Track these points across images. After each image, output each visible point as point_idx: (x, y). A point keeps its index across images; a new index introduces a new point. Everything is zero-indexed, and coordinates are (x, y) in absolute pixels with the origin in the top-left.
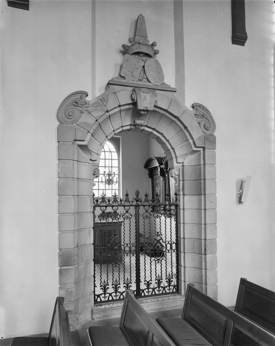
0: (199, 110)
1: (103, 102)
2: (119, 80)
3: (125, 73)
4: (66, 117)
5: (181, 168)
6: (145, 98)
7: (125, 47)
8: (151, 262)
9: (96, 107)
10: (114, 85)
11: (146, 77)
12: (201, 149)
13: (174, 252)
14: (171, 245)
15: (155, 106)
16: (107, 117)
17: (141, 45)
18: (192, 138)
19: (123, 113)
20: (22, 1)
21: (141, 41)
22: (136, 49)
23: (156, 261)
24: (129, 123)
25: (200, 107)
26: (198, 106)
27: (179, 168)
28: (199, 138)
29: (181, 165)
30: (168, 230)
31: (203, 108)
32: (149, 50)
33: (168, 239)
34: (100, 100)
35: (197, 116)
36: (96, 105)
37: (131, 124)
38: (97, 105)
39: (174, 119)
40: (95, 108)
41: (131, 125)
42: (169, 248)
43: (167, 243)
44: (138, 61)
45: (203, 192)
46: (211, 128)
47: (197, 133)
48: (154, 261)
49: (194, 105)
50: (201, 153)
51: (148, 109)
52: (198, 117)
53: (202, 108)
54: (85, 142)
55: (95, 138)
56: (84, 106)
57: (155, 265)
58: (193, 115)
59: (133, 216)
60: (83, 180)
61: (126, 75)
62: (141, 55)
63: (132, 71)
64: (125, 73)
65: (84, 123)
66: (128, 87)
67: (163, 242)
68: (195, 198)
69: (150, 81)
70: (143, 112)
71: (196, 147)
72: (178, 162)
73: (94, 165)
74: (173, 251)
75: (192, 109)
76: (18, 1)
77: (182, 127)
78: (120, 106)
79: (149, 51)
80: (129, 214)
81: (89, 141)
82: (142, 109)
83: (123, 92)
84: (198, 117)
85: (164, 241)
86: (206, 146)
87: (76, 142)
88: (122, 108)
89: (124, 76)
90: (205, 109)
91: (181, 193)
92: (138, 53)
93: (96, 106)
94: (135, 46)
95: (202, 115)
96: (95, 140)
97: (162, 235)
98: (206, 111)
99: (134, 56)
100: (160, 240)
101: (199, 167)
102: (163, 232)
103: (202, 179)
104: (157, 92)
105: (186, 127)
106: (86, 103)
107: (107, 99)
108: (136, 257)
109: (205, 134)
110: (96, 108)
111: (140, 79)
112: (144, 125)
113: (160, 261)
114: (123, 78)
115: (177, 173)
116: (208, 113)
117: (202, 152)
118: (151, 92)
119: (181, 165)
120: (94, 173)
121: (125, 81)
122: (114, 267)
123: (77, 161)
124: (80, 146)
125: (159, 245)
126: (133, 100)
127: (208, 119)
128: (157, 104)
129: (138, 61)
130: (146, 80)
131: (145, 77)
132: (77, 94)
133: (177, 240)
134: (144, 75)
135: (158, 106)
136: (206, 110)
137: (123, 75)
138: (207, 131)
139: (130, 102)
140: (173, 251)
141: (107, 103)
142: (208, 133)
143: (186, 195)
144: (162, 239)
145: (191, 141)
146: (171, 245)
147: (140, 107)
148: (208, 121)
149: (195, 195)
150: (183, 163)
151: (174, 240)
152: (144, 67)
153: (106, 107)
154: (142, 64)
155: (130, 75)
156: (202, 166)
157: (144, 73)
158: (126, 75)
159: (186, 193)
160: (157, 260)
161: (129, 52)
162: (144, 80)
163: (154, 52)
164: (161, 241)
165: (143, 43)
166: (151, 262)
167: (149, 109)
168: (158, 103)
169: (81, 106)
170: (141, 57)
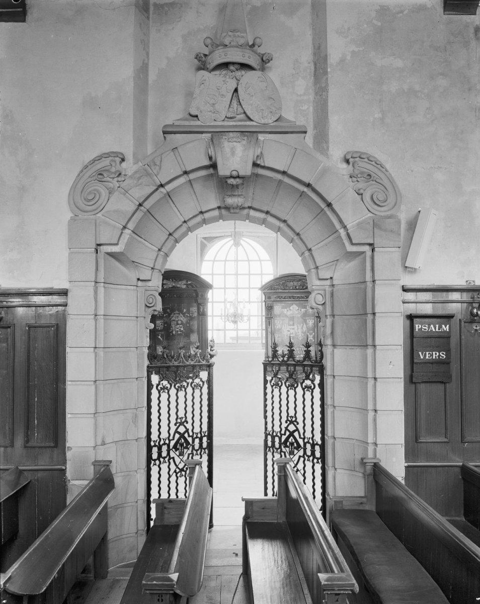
0: (361, 164)
1: (152, 168)
2: (187, 123)
3: (198, 108)
4: (91, 205)
5: (328, 289)
6: (233, 153)
7: (199, 58)
8: (170, 476)
9: (139, 178)
10: (175, 133)
11: (242, 111)
12: (367, 249)
13: (205, 452)
14: (201, 439)
15: (255, 165)
16: (162, 195)
17: (228, 49)
18: (345, 227)
19: (197, 187)
20: (12, 8)
21: (227, 42)
22: (219, 57)
23: (177, 474)
24: (216, 206)
25: (376, 163)
26: (356, 158)
27: (325, 290)
28: (360, 225)
29: (328, 282)
30: (308, 416)
31: (369, 160)
32: (247, 55)
33: (197, 430)
34: (146, 166)
35: (355, 179)
36: (138, 175)
37: (219, 205)
38: (142, 175)
39: (305, 189)
40: (135, 182)
41: (219, 208)
42: (164, 448)
43: (306, 440)
44: (223, 81)
45: (370, 342)
46: (388, 201)
47: (353, 214)
48: (175, 474)
49: (348, 157)
50: (365, 257)
51: (240, 174)
52: (357, 181)
53: (366, 160)
54: (119, 246)
55: (143, 237)
56: (116, 179)
57: (306, 479)
58: (347, 177)
59: (205, 383)
60: (121, 317)
61: (201, 112)
62: (232, 68)
63: (212, 101)
64: (198, 108)
65: (115, 211)
66: (203, 135)
67: (189, 436)
68: (358, 352)
69: (251, 117)
70: (232, 180)
71: (353, 244)
72: (321, 277)
73: (148, 288)
74: (315, 461)
75: (345, 165)
76: (8, 10)
77: (323, 205)
78: (186, 173)
79: (246, 58)
80: (199, 380)
81: (128, 245)
82: (228, 173)
83: (190, 145)
84: (358, 179)
85: (191, 434)
86: (377, 242)
87: (101, 247)
88: (192, 176)
89: (196, 114)
90: (373, 163)
91: (329, 342)
92: (225, 65)
93: (139, 177)
94: (217, 52)
95: (365, 176)
96: (144, 241)
97: (298, 424)
98: (377, 166)
99: (217, 72)
100: (294, 431)
101: (363, 286)
102: (300, 419)
103: (368, 312)
104: (261, 137)
105: (329, 205)
106: (120, 174)
107: (161, 161)
108: (208, 455)
109: (373, 215)
110: (139, 180)
111: (229, 115)
112: (246, 206)
113: (183, 473)
114: (196, 118)
115: (320, 299)
116: (382, 169)
117: (369, 253)
118: (245, 138)
119: (328, 282)
120: (148, 305)
121: (198, 123)
122: (179, 478)
123: (104, 283)
124: (111, 255)
125: (293, 441)
126: (210, 158)
127: (381, 182)
128: (264, 162)
129: (223, 81)
130: (243, 116)
131: (240, 110)
132: (103, 159)
133: (323, 439)
134: (239, 106)
135: (266, 165)
136: (375, 165)
137: (194, 113)
138: (376, 207)
139: (206, 162)
140: (203, 450)
141: (160, 168)
142: (382, 214)
143: (338, 347)
144: (297, 430)
145: (342, 232)
146: (313, 446)
147: (223, 171)
148: (385, 190)
149: (357, 347)
150: (331, 278)
151: (205, 428)
152: (236, 90)
153: (158, 177)
154: (232, 85)
155: (209, 110)
156: (370, 285)
157: (238, 103)
158: (201, 112)
159: (338, 341)
160: (179, 472)
161: (208, 66)
162: (238, 116)
163: (258, 57)
164: (186, 435)
165: (232, 43)
166: (170, 476)
167: (242, 173)
168: (265, 159)
169: (111, 180)
170: (232, 72)
